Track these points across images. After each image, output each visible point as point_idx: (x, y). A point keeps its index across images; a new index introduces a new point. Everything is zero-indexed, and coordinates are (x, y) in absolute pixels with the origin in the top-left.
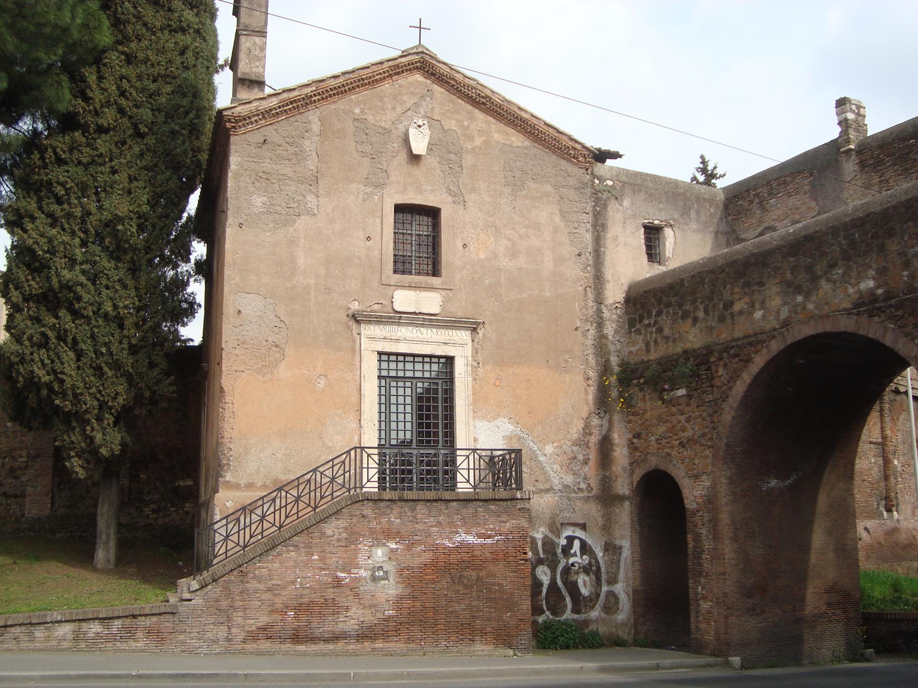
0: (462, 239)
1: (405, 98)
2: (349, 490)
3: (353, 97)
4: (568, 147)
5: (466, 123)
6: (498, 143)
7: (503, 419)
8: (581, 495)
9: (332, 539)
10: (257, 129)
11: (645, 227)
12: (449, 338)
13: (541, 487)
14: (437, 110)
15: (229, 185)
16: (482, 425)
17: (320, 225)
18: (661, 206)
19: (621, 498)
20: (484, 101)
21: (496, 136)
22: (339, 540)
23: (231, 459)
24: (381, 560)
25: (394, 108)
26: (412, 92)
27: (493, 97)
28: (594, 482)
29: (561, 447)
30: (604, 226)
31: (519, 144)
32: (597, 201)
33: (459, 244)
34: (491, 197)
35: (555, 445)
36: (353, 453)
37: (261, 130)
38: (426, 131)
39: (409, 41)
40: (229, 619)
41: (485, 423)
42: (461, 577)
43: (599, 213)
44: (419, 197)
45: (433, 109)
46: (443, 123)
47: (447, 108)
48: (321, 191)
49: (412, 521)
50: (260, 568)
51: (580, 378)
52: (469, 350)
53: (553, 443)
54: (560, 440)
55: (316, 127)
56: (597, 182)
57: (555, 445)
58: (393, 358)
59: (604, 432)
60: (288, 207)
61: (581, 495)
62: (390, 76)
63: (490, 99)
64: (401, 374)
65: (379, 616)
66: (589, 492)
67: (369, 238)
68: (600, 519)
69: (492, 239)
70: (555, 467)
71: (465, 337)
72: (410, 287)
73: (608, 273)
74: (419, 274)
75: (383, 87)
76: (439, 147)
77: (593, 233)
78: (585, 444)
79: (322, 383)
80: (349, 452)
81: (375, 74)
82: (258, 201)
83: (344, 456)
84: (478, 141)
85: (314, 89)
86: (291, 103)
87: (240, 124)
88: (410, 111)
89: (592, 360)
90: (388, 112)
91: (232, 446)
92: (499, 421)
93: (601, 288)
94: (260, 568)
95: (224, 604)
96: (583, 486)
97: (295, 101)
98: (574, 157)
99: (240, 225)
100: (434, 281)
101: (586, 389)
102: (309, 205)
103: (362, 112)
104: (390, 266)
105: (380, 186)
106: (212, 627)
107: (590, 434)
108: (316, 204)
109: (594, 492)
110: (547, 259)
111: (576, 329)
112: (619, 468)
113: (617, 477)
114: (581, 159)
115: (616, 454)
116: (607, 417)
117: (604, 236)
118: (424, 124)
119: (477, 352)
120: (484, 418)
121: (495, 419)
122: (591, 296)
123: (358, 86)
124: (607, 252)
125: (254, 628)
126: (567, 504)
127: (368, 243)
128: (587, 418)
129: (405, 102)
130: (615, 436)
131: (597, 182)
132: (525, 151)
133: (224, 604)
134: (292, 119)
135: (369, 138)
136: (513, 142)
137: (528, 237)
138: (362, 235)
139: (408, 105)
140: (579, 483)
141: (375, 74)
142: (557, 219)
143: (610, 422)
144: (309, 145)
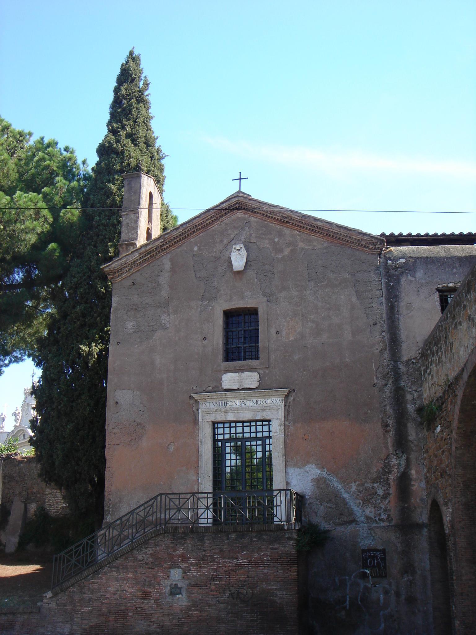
0: (275, 328)
1: (230, 232)
2: (156, 527)
3: (192, 240)
4: (359, 240)
5: (276, 240)
6: (302, 249)
7: (311, 465)
8: (382, 524)
9: (142, 562)
10: (130, 276)
11: (439, 290)
12: (267, 405)
13: (345, 519)
14: (253, 235)
15: (111, 317)
16: (294, 472)
17: (170, 335)
18: (455, 270)
19: (420, 526)
20: (287, 220)
21: (301, 245)
22: (146, 563)
23: (111, 506)
24: (177, 579)
25: (222, 241)
26: (234, 226)
27: (293, 216)
28: (394, 513)
29: (362, 485)
30: (396, 297)
31: (320, 246)
32: (389, 277)
33: (273, 331)
34: (298, 291)
35: (358, 483)
36: (159, 498)
37: (131, 276)
38: (244, 253)
39: (230, 190)
40: (72, 619)
41: (297, 469)
42: (238, 593)
43: (392, 287)
44: (241, 302)
45: (250, 235)
46: (258, 243)
47: (261, 232)
48: (171, 311)
49: (200, 549)
50: (93, 583)
51: (378, 428)
52: (281, 414)
53: (355, 482)
54: (361, 480)
55: (167, 265)
56: (390, 262)
57: (358, 483)
58: (227, 425)
59: (402, 470)
60: (149, 326)
61: (382, 524)
62: (217, 219)
63: (291, 217)
64: (253, 435)
65: (175, 621)
66: (390, 522)
67: (205, 339)
68: (399, 545)
69: (300, 324)
70: (358, 501)
71: (279, 403)
72: (235, 371)
73: (403, 335)
74: (245, 359)
75: (213, 228)
76: (256, 262)
77: (387, 305)
78: (384, 481)
79: (172, 448)
80: (156, 498)
81: (205, 220)
82: (130, 325)
83: (153, 501)
84: (287, 251)
85: (162, 240)
86: (148, 254)
87: (117, 275)
88: (234, 241)
89: (389, 410)
90: (218, 245)
91: (111, 497)
92: (308, 467)
93: (397, 348)
94: (93, 583)
95: (69, 608)
96: (383, 516)
97: (151, 252)
98: (365, 247)
99: (118, 343)
100: (254, 363)
101: (384, 434)
102: (163, 322)
103: (199, 249)
104: (221, 356)
105: (213, 298)
106: (61, 624)
107: (390, 473)
108: (168, 320)
109: (393, 523)
110: (346, 332)
111: (374, 385)
112: (418, 500)
113: (415, 508)
114: (371, 247)
115: (414, 488)
116: (404, 456)
117: (398, 305)
118: (241, 248)
119: (288, 414)
120: (296, 465)
121: (305, 466)
122: (386, 355)
123: (194, 231)
124: (401, 318)
125: (87, 627)
126: (368, 533)
127: (204, 342)
128: (386, 459)
129: (230, 235)
130: (413, 472)
131: (390, 262)
132: (325, 251)
133: (69, 608)
134: (151, 265)
135: (204, 266)
136: (315, 246)
137: (330, 317)
138: (200, 337)
139: (232, 237)
140: (380, 515)
141: (205, 220)
142: (354, 299)
143: (408, 460)
144: (164, 279)
